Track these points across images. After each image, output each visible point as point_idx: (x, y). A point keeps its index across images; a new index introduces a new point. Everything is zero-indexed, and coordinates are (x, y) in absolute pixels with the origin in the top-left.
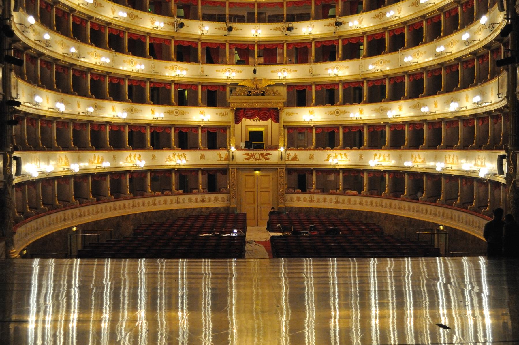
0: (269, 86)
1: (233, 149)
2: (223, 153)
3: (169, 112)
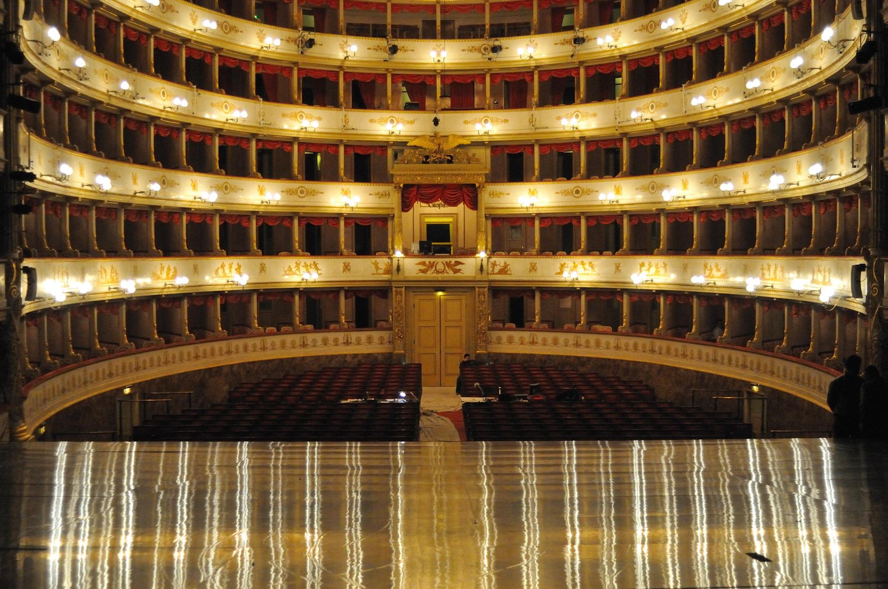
0: (461, 146)
3: (290, 192)
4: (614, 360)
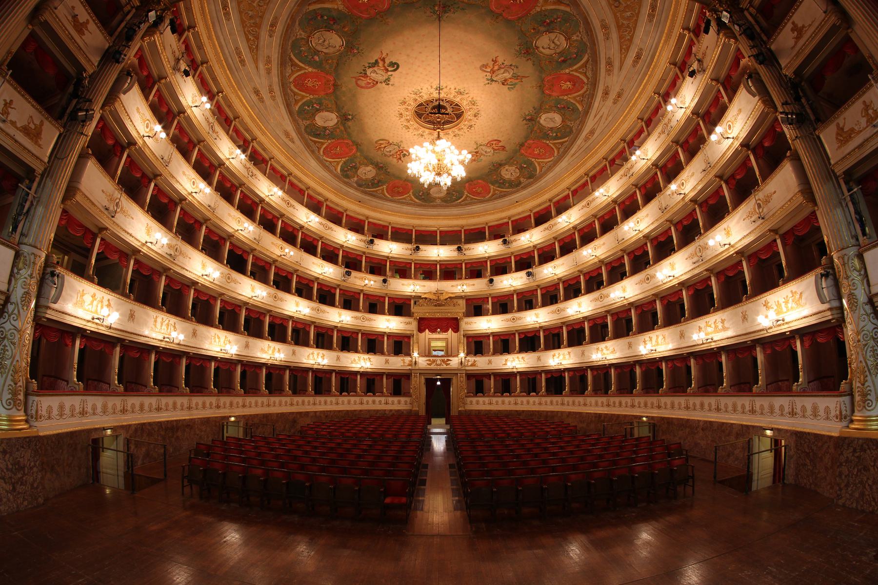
0: (450, 298)
2: (407, 359)
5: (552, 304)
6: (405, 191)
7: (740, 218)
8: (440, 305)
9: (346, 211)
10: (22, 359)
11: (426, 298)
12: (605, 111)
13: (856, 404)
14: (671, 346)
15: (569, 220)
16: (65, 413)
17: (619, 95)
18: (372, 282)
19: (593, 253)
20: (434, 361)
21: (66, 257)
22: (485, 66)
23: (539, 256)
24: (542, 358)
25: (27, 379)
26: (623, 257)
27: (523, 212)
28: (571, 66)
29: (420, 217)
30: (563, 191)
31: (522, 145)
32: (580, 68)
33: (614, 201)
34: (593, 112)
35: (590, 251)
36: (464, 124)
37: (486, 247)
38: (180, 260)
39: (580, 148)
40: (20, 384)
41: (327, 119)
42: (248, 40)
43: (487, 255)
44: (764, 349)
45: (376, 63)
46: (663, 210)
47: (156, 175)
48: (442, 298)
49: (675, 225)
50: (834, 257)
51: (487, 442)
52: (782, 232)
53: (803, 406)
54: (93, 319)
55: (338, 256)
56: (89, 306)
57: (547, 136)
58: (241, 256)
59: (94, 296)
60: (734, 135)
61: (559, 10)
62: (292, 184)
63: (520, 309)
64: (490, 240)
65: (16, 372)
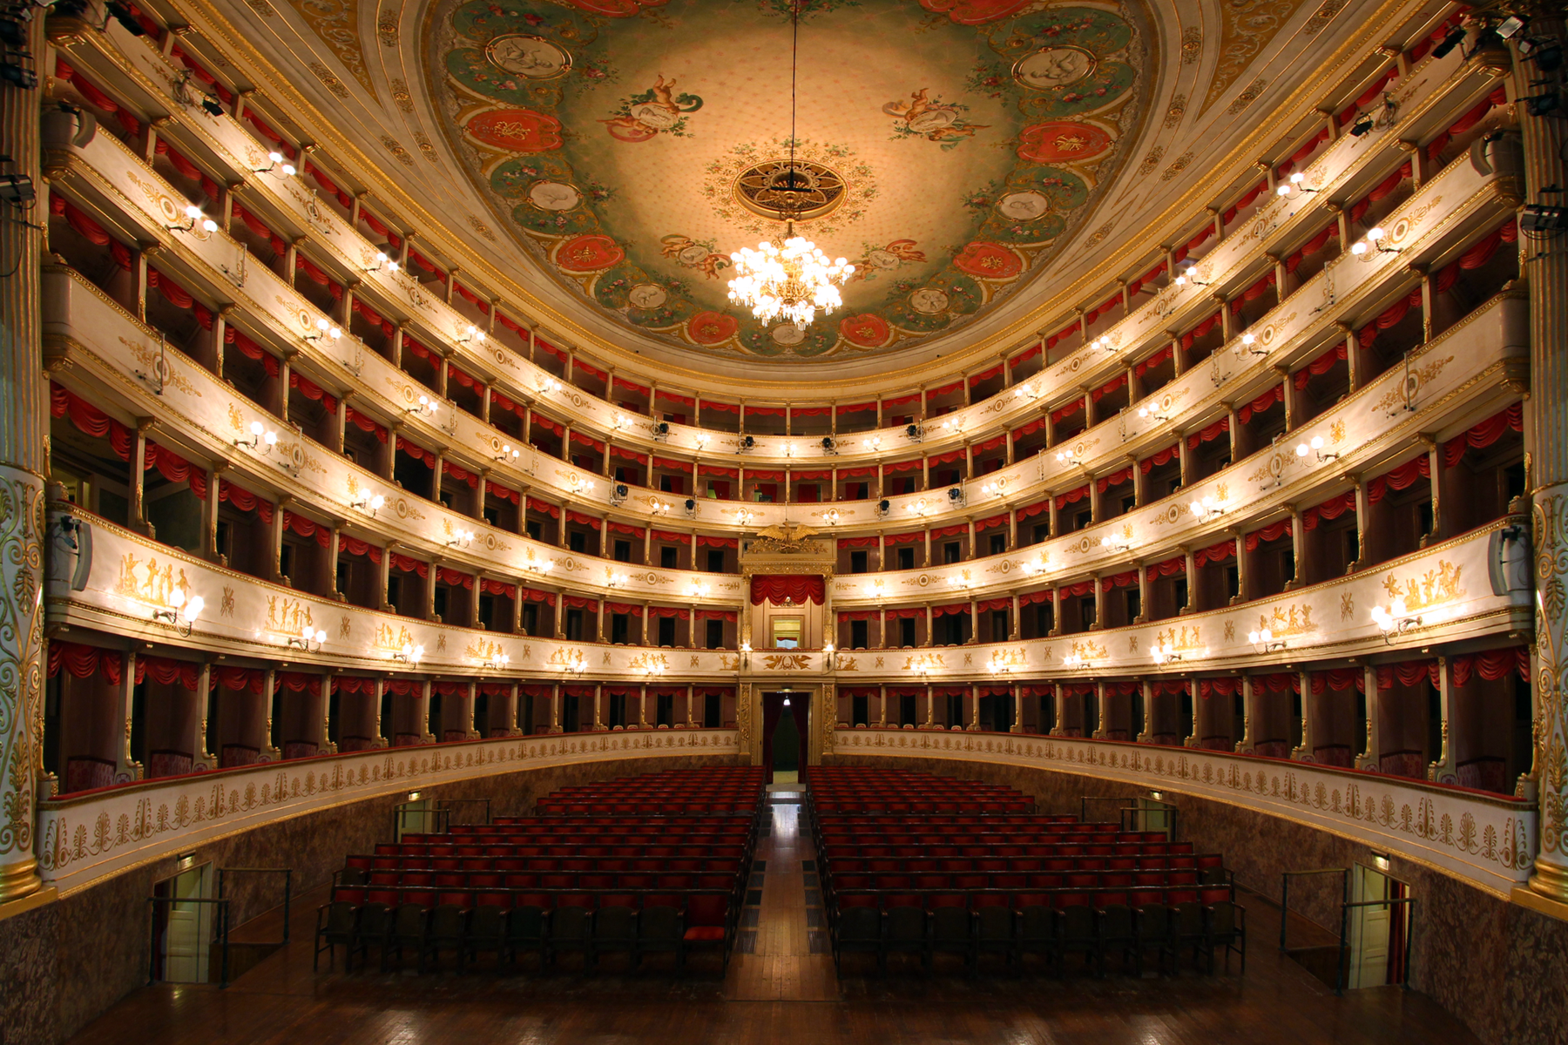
0: (810, 537)
1: (746, 647)
3: (639, 577)
4: (966, 763)
5: (994, 552)
6: (725, 332)
7: (1366, 407)
8: (790, 551)
9: (612, 369)
10: (29, 728)
11: (765, 538)
12: (1141, 191)
13: (1543, 831)
14: (1207, 652)
15: (1036, 392)
16: (121, 833)
17: (1180, 165)
18: (667, 508)
19: (1074, 458)
20: (779, 660)
21: (86, 486)
22: (896, 106)
23: (975, 459)
24: (973, 658)
25: (39, 772)
26: (1131, 467)
27: (949, 375)
28: (1088, 108)
29: (754, 381)
30: (1030, 338)
31: (957, 251)
32: (1107, 113)
33: (1127, 361)
34: (1116, 194)
35: (1069, 454)
36: (841, 209)
37: (876, 441)
38: (306, 476)
39: (1074, 259)
40: (27, 787)
41: (556, 196)
42: (337, 51)
43: (877, 456)
44: (1379, 678)
45: (650, 96)
46: (1218, 382)
47: (224, 306)
48: (795, 536)
49: (1238, 413)
50: (1536, 498)
51: (875, 819)
52: (1444, 438)
53: (1446, 817)
54: (156, 616)
55: (602, 456)
56: (147, 589)
57: (1011, 236)
58: (420, 464)
59: (152, 566)
60: (1404, 245)
61: (1090, 9)
62: (501, 318)
63: (937, 562)
64: (884, 426)
65: (18, 761)
